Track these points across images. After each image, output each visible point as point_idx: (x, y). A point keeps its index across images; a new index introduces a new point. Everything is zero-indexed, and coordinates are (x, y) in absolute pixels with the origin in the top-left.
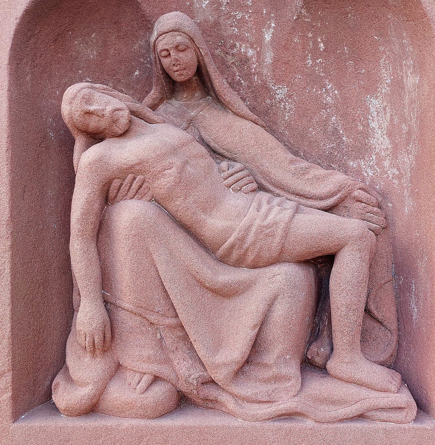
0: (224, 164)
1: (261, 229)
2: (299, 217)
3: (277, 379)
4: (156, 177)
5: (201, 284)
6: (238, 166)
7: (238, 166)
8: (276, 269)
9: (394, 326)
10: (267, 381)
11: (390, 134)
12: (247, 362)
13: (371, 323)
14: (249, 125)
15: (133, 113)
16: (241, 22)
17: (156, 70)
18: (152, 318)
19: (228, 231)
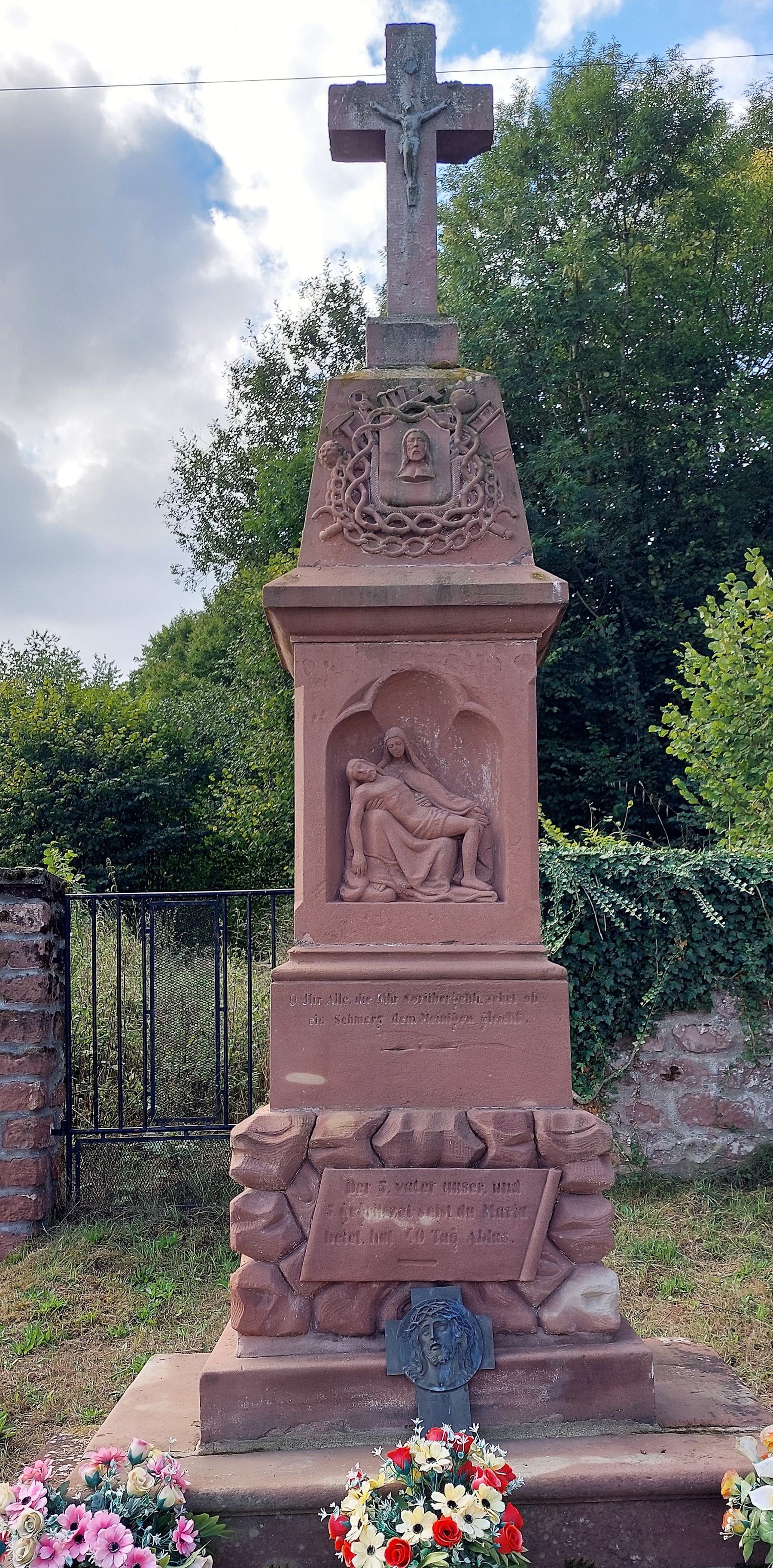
0: (416, 794)
1: (434, 821)
2: (449, 817)
3: (439, 886)
4: (388, 799)
5: (406, 845)
6: (423, 795)
7: (423, 795)
8: (439, 839)
9: (491, 868)
10: (434, 887)
11: (491, 783)
12: (426, 880)
13: (481, 866)
14: (427, 777)
15: (377, 772)
16: (424, 729)
17: (386, 752)
18: (385, 860)
19: (420, 822)
